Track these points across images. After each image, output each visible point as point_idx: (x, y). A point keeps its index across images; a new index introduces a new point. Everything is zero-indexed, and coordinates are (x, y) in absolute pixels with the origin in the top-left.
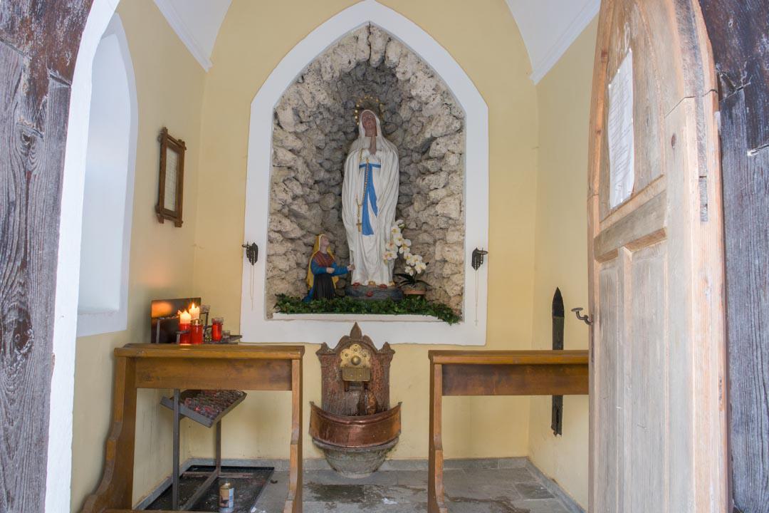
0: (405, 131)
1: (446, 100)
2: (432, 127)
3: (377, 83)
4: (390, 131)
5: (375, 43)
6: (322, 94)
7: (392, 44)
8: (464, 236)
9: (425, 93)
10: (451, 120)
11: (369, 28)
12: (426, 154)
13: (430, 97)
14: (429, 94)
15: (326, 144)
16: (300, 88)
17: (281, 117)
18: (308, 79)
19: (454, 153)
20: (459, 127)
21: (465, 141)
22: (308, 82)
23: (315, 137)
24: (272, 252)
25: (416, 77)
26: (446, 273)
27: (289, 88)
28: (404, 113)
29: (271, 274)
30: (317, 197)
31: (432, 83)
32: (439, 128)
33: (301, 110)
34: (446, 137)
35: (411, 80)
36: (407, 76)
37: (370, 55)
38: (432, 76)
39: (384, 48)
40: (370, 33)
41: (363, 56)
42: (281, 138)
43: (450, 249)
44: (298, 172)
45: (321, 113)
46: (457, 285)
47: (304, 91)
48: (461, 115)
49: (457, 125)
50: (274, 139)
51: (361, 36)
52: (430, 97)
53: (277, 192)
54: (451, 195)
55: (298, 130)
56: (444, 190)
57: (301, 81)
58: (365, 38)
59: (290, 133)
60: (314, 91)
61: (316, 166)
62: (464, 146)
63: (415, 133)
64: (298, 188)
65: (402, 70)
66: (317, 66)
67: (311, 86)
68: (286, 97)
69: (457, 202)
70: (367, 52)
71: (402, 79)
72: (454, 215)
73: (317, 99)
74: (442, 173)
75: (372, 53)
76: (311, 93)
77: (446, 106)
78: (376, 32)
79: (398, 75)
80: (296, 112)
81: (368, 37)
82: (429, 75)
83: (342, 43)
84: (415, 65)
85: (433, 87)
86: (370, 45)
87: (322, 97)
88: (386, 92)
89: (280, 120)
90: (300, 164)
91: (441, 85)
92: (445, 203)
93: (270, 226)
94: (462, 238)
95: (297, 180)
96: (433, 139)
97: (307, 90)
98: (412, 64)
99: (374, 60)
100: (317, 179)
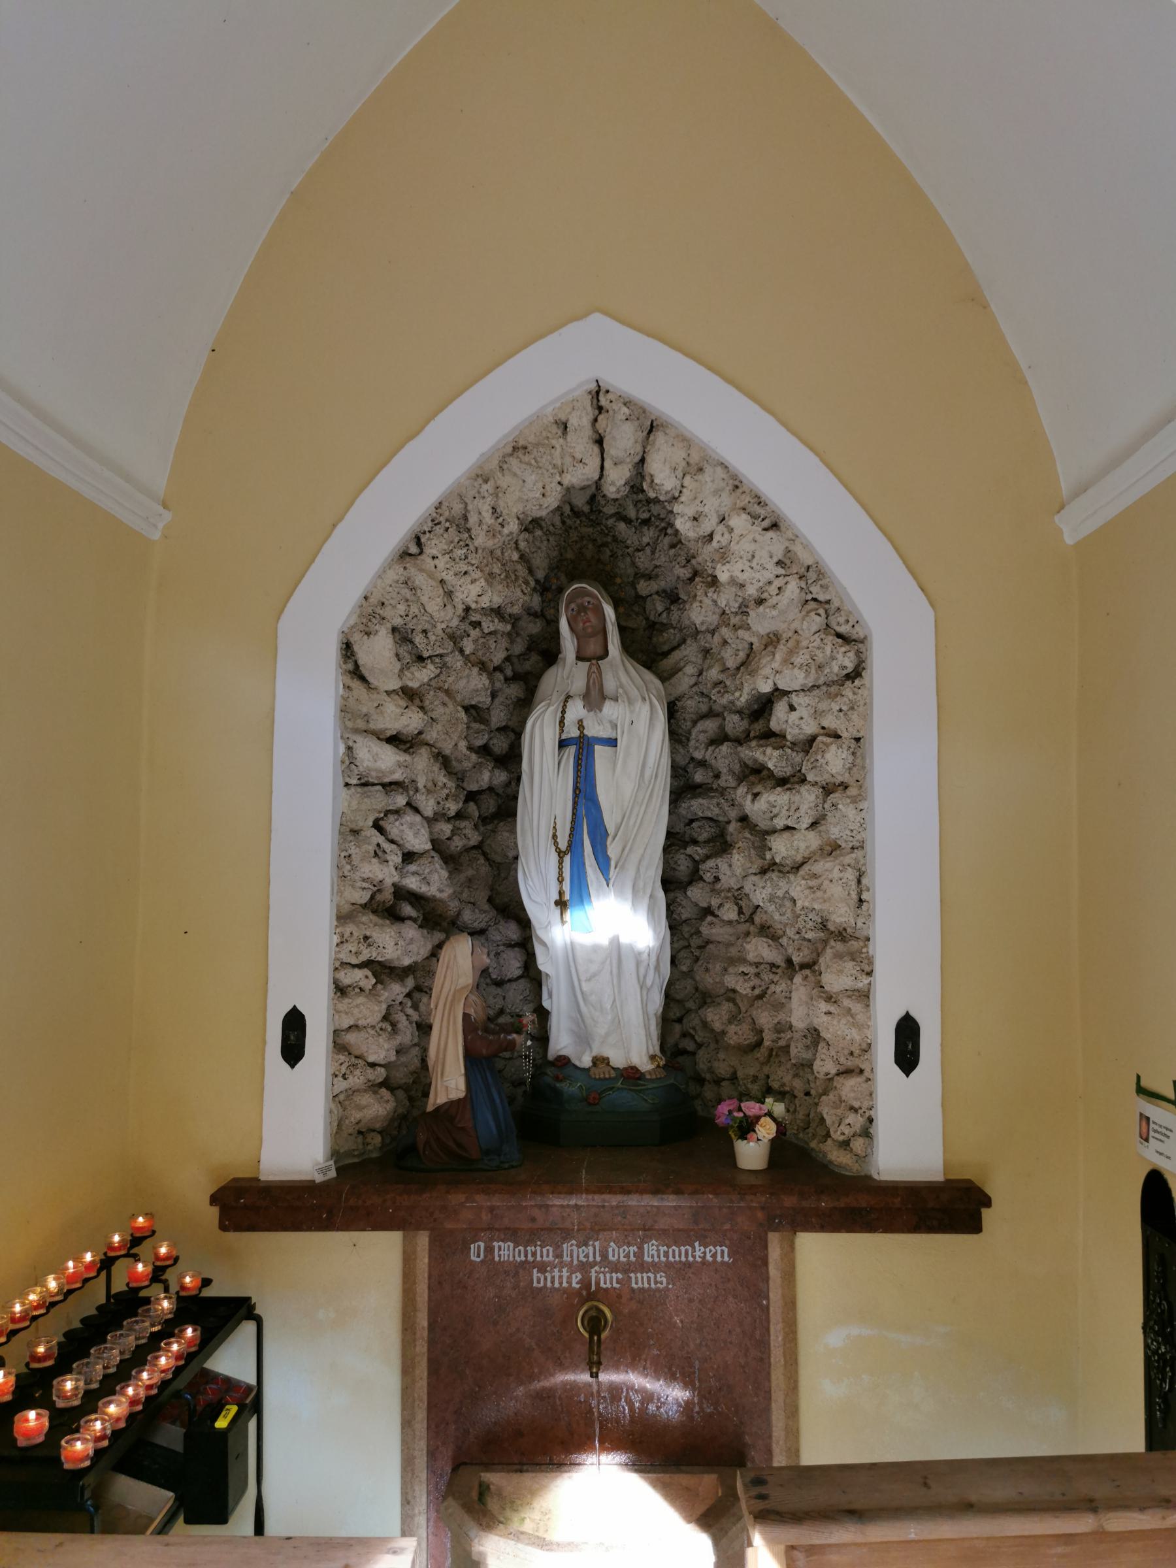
0: (706, 652)
1: (813, 589)
2: (776, 665)
3: (628, 521)
4: (666, 648)
5: (614, 438)
6: (473, 581)
7: (659, 438)
8: (870, 974)
9: (757, 576)
10: (828, 649)
11: (597, 393)
12: (761, 722)
13: (770, 583)
14: (769, 575)
15: (494, 695)
16: (412, 571)
17: (364, 657)
18: (435, 545)
19: (837, 736)
20: (850, 666)
21: (868, 704)
22: (434, 552)
23: (463, 683)
24: (346, 1022)
25: (731, 530)
26: (825, 1070)
27: (380, 576)
28: (700, 613)
29: (341, 1085)
30: (474, 838)
31: (774, 545)
32: (796, 671)
33: (419, 628)
34: (816, 692)
35: (716, 537)
36: (708, 525)
37: (602, 468)
38: (775, 526)
39: (639, 448)
40: (600, 409)
41: (582, 474)
42: (365, 710)
43: (832, 1009)
44: (417, 790)
45: (476, 625)
46: (854, 1110)
47: (420, 579)
48: (858, 632)
49: (848, 662)
50: (344, 710)
51: (573, 422)
52: (770, 583)
53: (356, 859)
54: (832, 849)
55: (410, 684)
56: (811, 835)
57: (414, 549)
58: (586, 421)
59: (388, 693)
60: (449, 577)
61: (468, 759)
62: (867, 717)
63: (731, 663)
64: (416, 834)
65: (690, 511)
66: (458, 508)
67: (442, 562)
68: (372, 600)
69: (850, 875)
70: (593, 463)
71: (692, 535)
72: (841, 915)
73: (459, 596)
74: (804, 789)
75: (607, 464)
76: (442, 581)
77: (812, 605)
78: (615, 406)
79: (679, 524)
80: (402, 636)
81: (596, 420)
82: (766, 523)
83: (521, 443)
84: (725, 495)
85: (779, 555)
86: (600, 441)
87: (475, 590)
88: (654, 546)
89: (360, 662)
90: (422, 766)
91: (797, 548)
92: (815, 876)
93: (337, 953)
94: (866, 980)
95: (417, 810)
96: (779, 693)
97: (431, 576)
98: (717, 492)
99: (613, 483)
100: (474, 787)
